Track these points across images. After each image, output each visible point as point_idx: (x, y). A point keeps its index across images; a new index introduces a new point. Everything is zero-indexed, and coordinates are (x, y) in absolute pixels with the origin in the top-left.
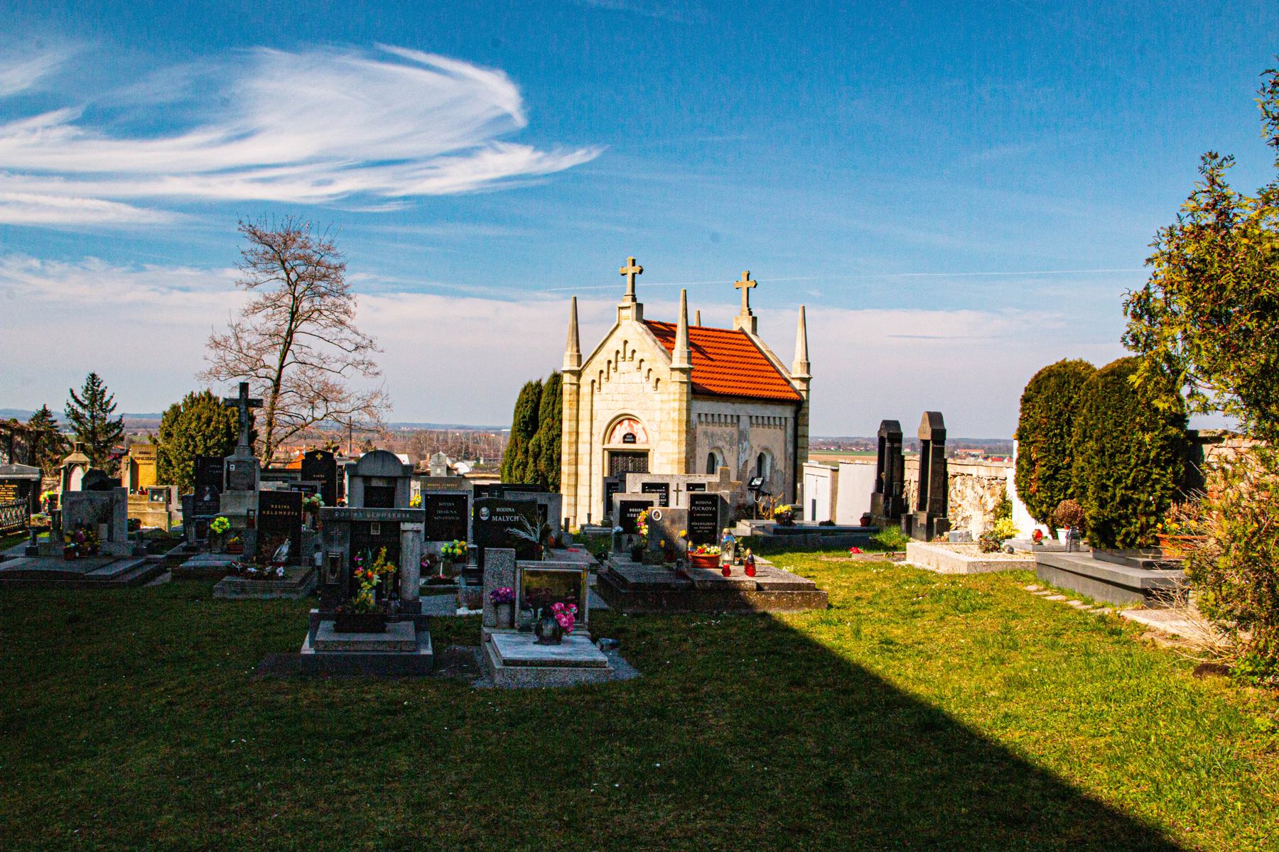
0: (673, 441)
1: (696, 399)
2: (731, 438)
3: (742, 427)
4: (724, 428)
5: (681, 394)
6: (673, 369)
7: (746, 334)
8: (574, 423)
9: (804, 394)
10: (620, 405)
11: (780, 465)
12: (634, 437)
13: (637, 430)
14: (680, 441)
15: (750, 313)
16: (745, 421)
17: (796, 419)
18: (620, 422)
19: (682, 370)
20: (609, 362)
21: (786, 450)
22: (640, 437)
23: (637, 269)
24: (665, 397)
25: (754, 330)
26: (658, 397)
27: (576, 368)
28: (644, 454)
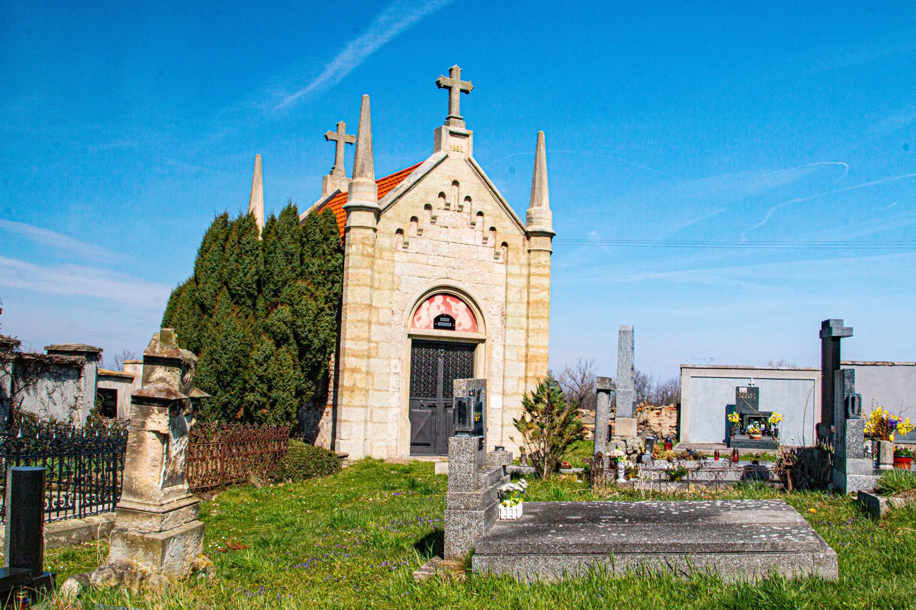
12: (452, 321)
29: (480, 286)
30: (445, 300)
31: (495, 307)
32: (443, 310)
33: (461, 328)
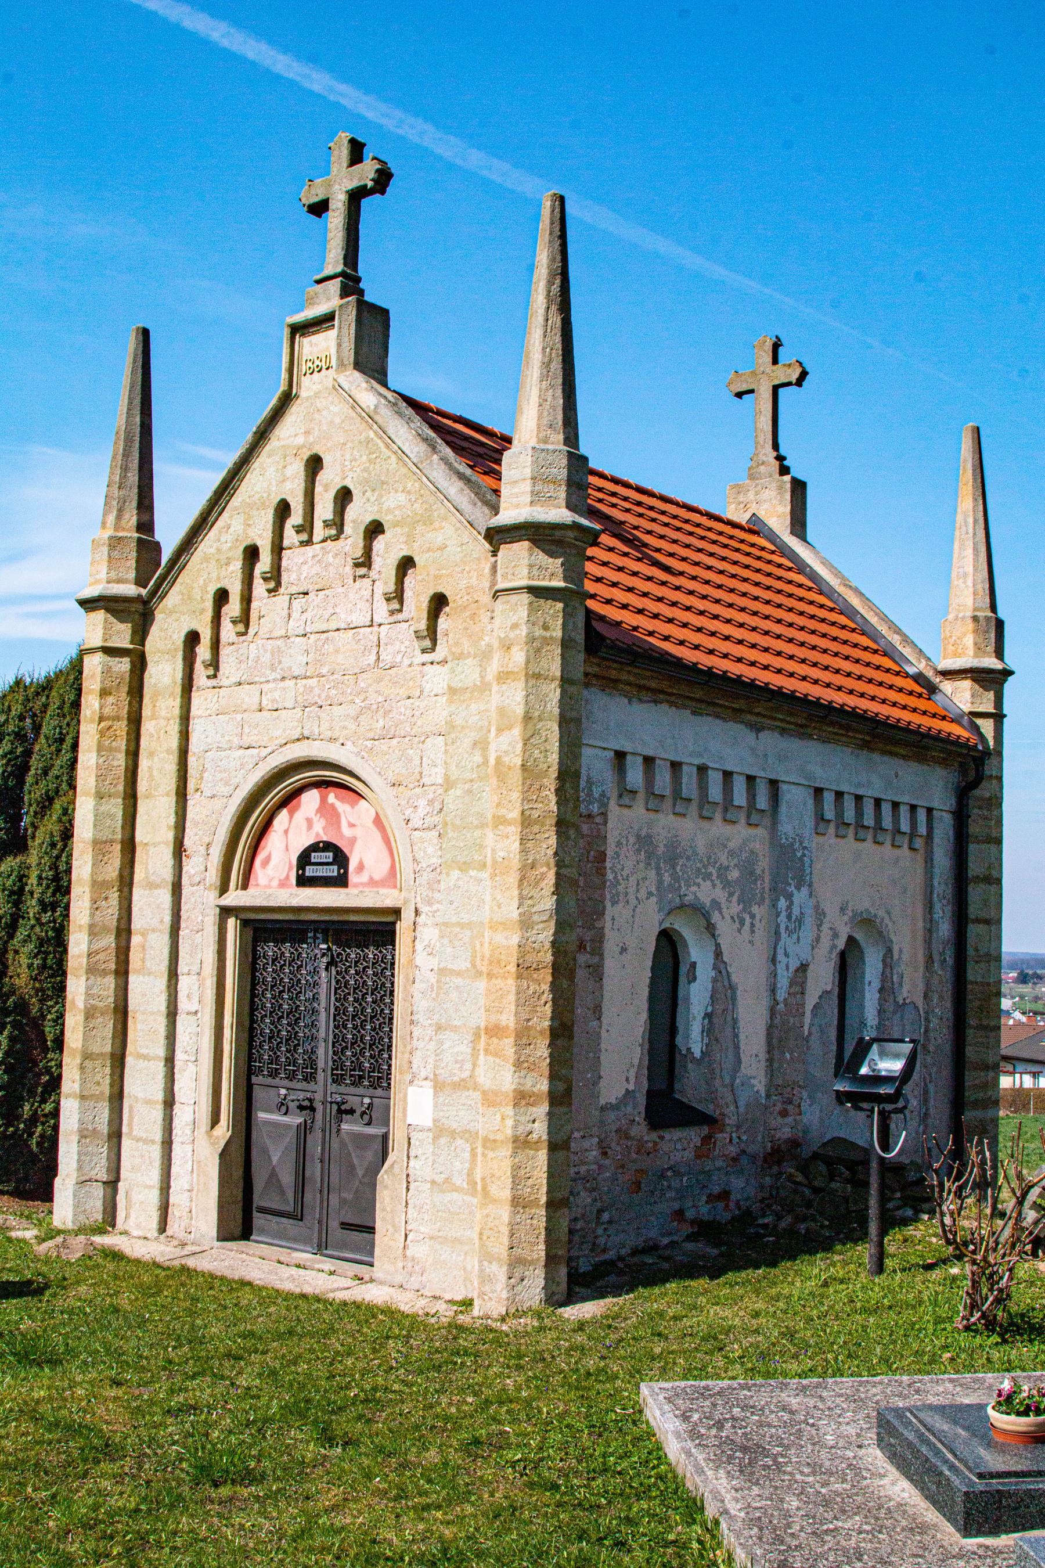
0: (498, 869)
1: (609, 684)
2: (749, 870)
3: (786, 828)
4: (718, 828)
5: (535, 647)
6: (498, 537)
7: (772, 537)
8: (116, 807)
9: (987, 727)
10: (288, 724)
11: (911, 985)
12: (341, 859)
13: (354, 825)
14: (527, 867)
15: (784, 470)
16: (797, 809)
17: (960, 817)
18: (289, 799)
19: (539, 534)
20: (252, 554)
21: (929, 931)
22: (366, 856)
23: (366, 172)
24: (469, 672)
25: (799, 524)
26: (437, 679)
27: (130, 590)
28: (377, 931)
29: (383, 746)
30: (323, 799)
31: (422, 803)
32: (320, 832)
33: (364, 878)
